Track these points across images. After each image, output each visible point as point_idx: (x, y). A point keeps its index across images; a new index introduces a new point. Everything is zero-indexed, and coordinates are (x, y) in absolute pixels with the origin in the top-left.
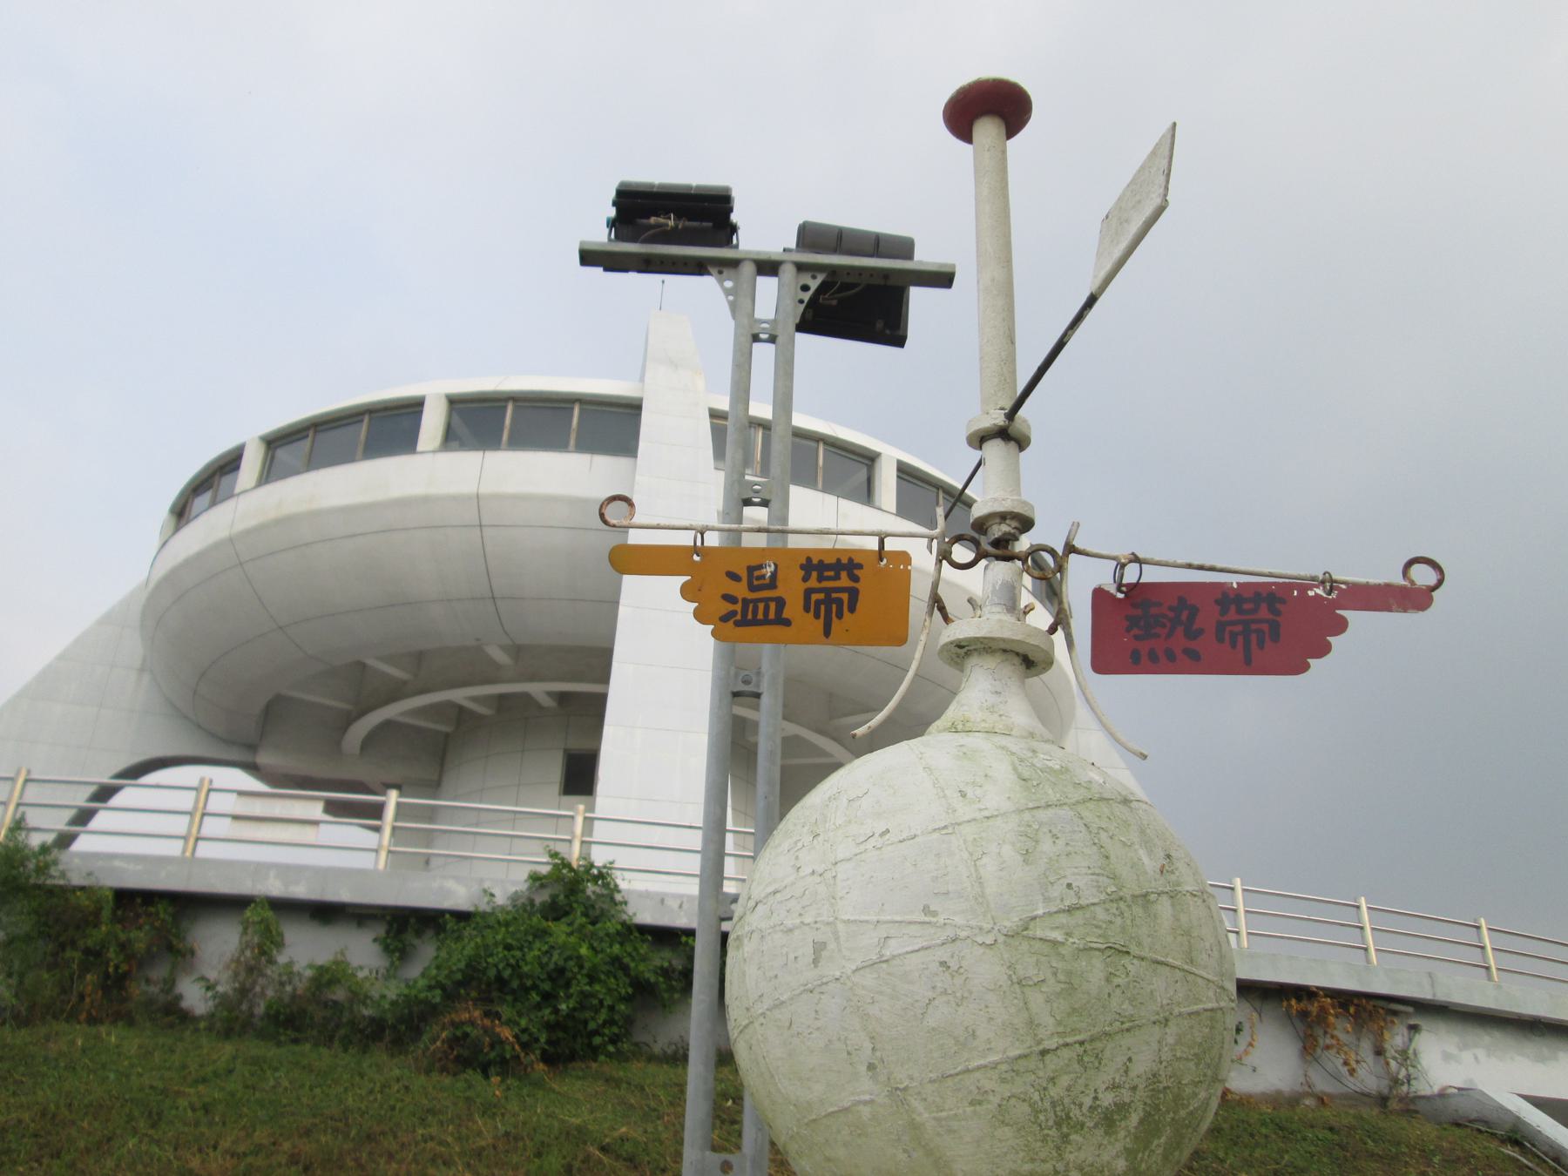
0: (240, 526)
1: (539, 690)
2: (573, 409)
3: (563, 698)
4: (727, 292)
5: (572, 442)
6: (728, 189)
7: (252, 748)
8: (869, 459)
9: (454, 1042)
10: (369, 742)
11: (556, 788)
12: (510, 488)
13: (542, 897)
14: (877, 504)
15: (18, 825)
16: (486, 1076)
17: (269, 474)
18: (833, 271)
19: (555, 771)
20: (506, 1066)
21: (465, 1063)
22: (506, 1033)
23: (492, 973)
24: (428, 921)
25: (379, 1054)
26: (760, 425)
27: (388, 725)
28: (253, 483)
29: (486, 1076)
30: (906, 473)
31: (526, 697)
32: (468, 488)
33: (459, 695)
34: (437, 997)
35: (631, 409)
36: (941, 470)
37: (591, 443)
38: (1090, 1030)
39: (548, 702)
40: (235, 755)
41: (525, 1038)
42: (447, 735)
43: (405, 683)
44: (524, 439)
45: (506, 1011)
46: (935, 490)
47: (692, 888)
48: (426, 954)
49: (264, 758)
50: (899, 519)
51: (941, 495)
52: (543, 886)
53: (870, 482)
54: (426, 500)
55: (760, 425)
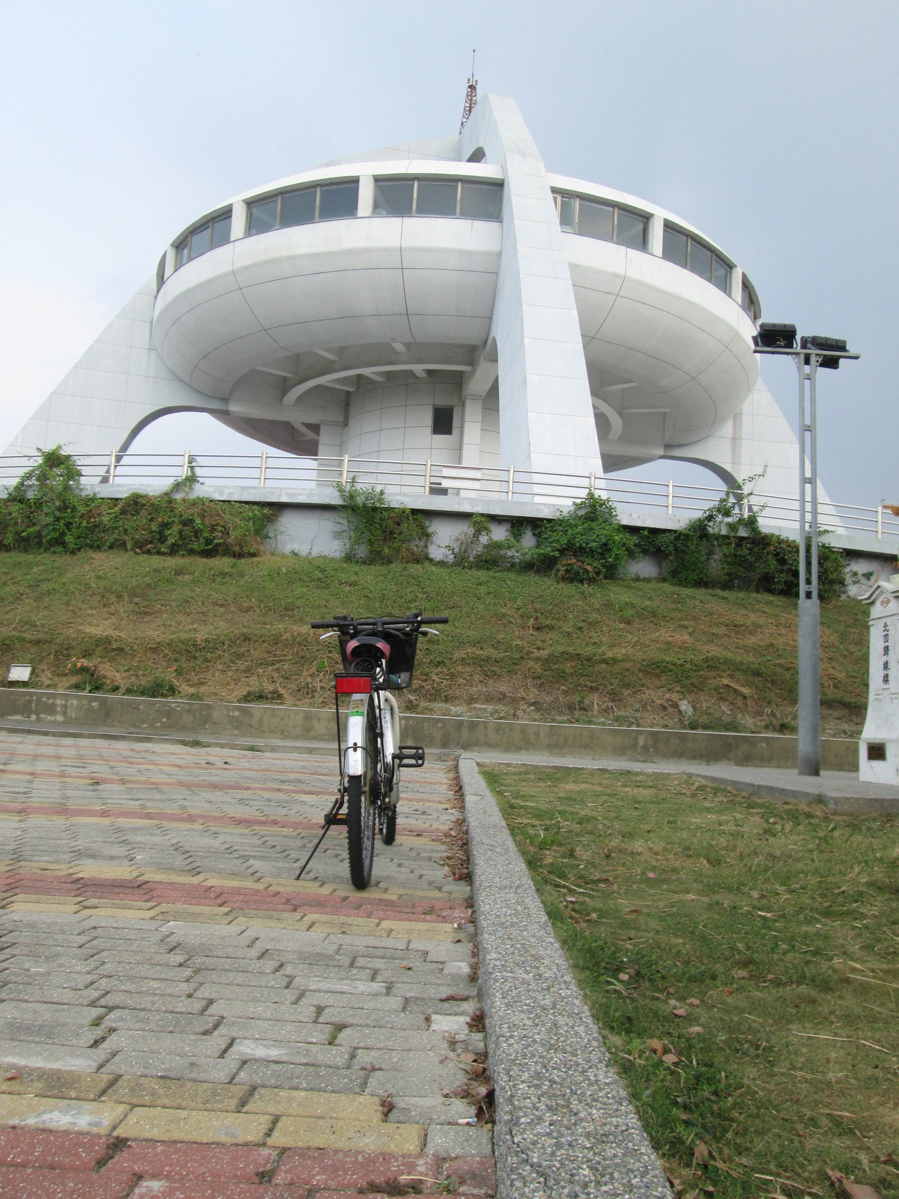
0: (238, 265)
1: (418, 369)
2: (457, 186)
3: (430, 372)
4: (796, 363)
5: (458, 211)
6: (793, 326)
7: (225, 400)
8: (646, 218)
9: (567, 571)
10: (300, 398)
11: (429, 430)
12: (422, 243)
13: (582, 513)
14: (650, 250)
15: (60, 447)
16: (582, 584)
17: (255, 226)
18: (825, 356)
19: (428, 419)
20: (592, 581)
21: (571, 580)
22: (589, 568)
23: (578, 545)
24: (535, 524)
25: (532, 578)
26: (577, 196)
27: (319, 387)
28: (241, 235)
29: (582, 584)
30: (669, 226)
31: (411, 373)
32: (394, 243)
33: (366, 371)
34: (557, 554)
35: (497, 186)
36: (705, 233)
37: (474, 212)
38: (650, 599)
39: (424, 375)
40: (216, 405)
41: (596, 570)
42: (348, 393)
43: (333, 362)
44: (426, 209)
45: (588, 560)
46: (685, 238)
47: (797, 525)
48: (528, 540)
49: (234, 408)
50: (664, 261)
51: (689, 241)
52: (580, 508)
53: (645, 231)
54: (368, 250)
55: (577, 196)
